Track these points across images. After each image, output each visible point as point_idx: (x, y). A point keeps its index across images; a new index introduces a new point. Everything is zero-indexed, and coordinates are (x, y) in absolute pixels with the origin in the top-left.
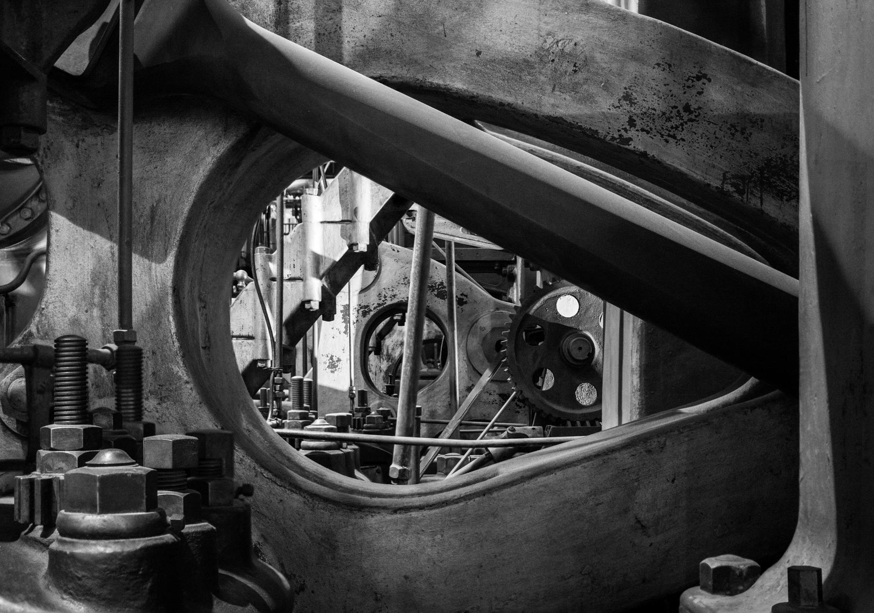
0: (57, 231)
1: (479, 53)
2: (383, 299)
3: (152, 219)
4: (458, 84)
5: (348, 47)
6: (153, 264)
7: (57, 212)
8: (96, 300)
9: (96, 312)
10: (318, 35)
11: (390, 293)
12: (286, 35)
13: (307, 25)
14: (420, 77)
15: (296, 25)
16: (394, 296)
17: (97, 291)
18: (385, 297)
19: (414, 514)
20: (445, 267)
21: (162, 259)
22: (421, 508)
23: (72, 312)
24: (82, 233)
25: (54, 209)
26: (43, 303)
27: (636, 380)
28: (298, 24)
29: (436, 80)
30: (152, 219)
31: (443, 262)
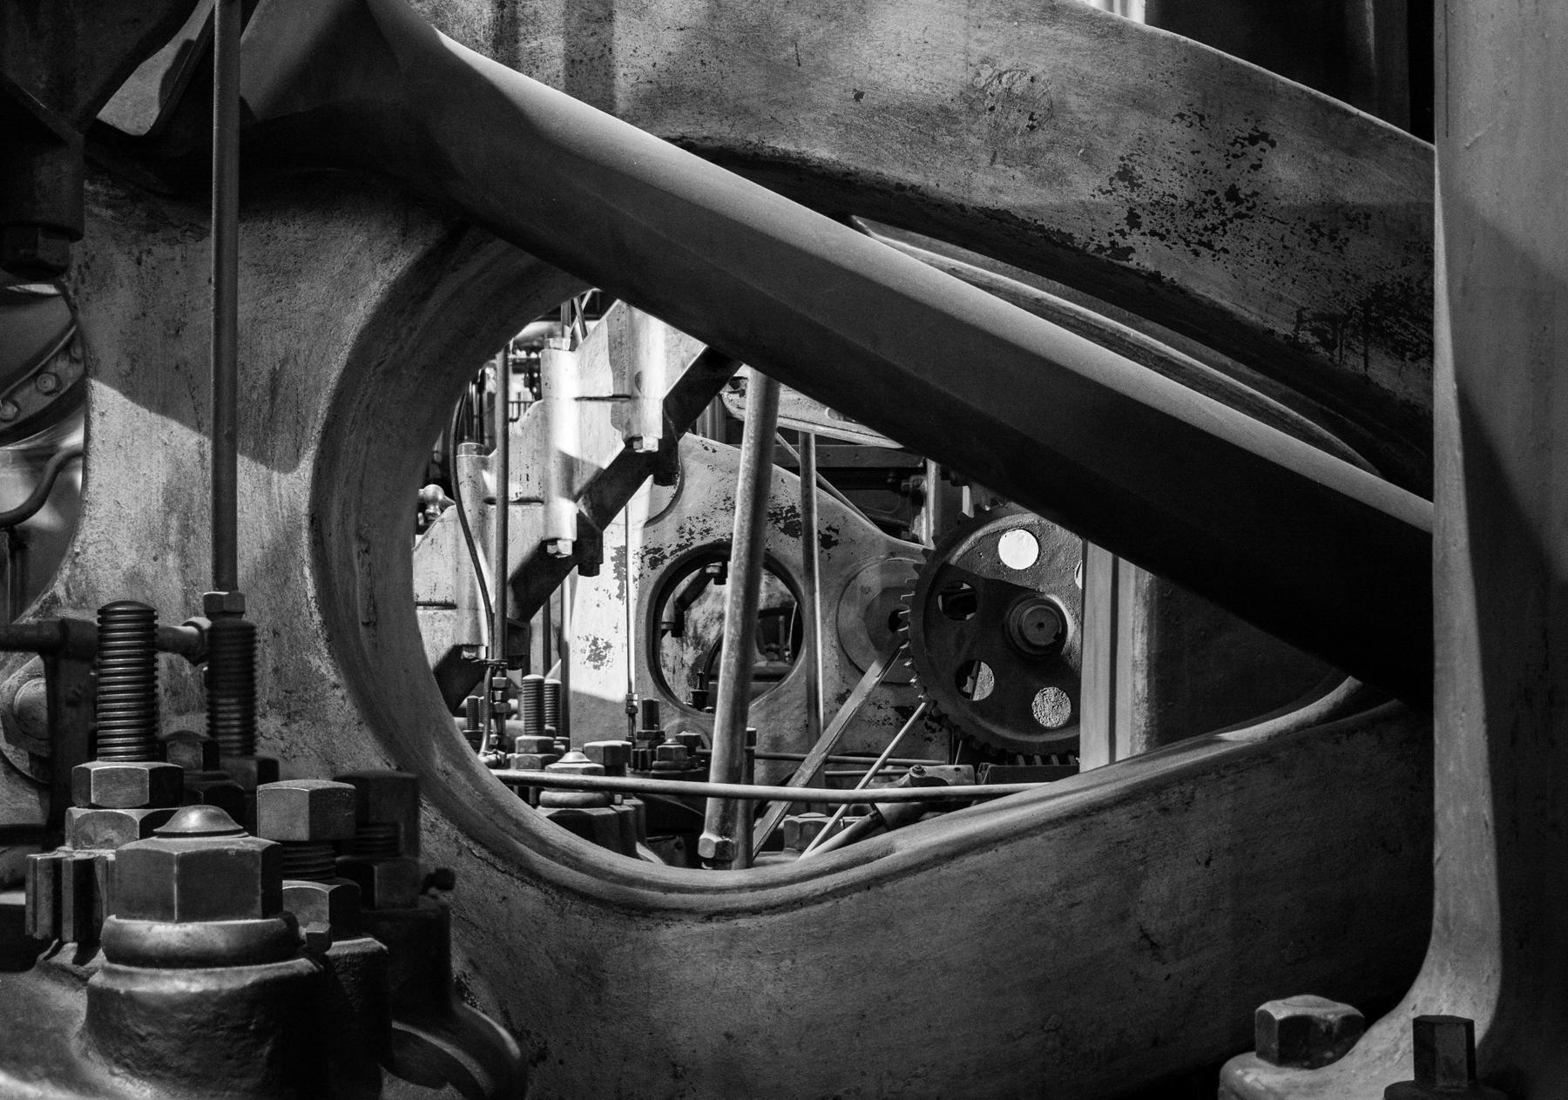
0: (103, 414)
1: (859, 96)
2: (688, 536)
3: (273, 392)
4: (822, 151)
5: (624, 85)
6: (275, 474)
7: (102, 380)
8: (172, 539)
9: (172, 560)
10: (571, 63)
11: (699, 526)
12: (513, 63)
13: (551, 44)
14: (753, 138)
15: (531, 44)
16: (708, 531)
17: (174, 523)
18: (691, 533)
19: (743, 922)
20: (798, 478)
21: (290, 465)
22: (755, 911)
23: (129, 559)
24: (146, 418)
25: (96, 375)
26: (78, 544)
27: (1141, 683)
28: (534, 44)
29: (783, 144)
30: (273, 392)
31: (795, 470)
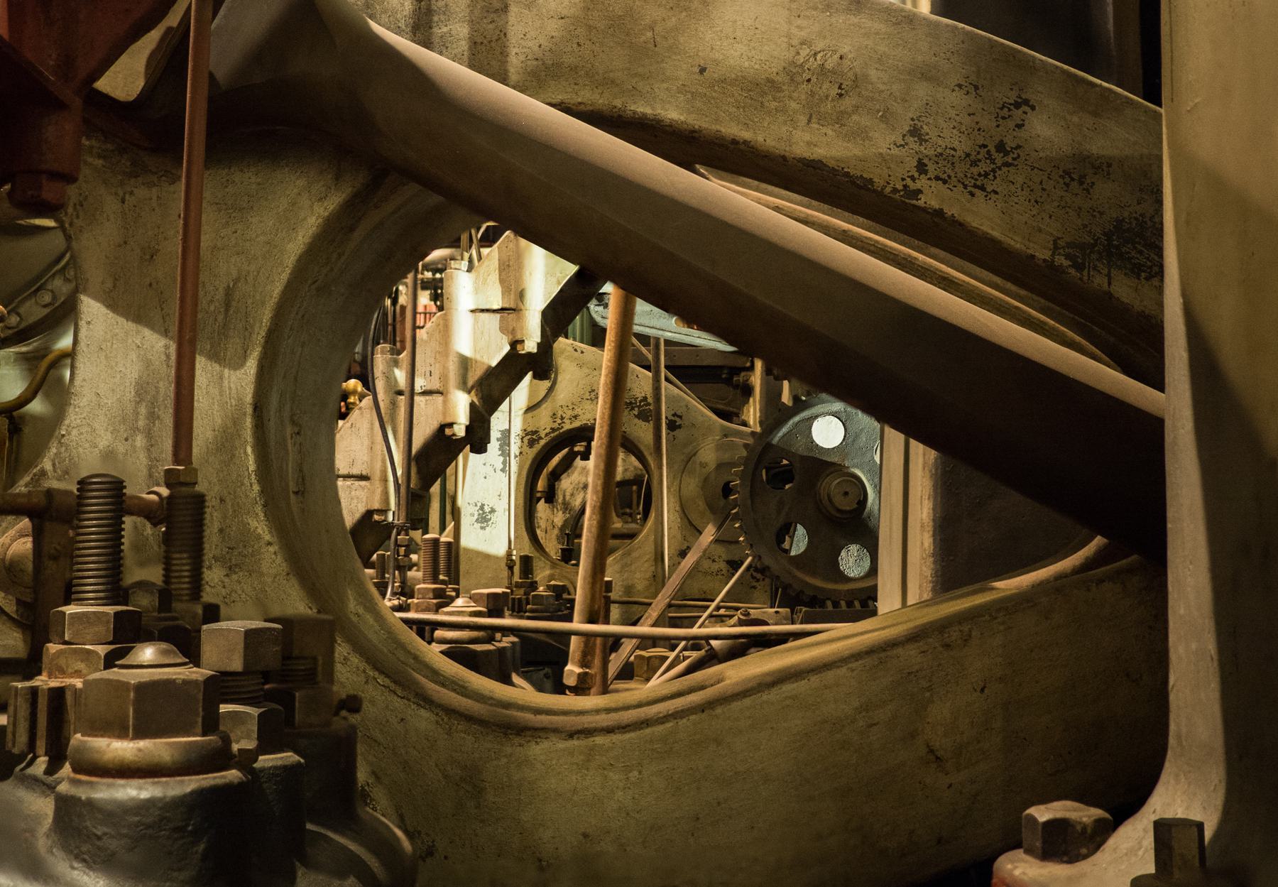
0: (89, 323)
1: (702, 70)
2: (559, 421)
3: (227, 306)
4: (673, 113)
5: (515, 62)
7: (89, 296)
8: (141, 423)
9: (140, 441)
10: (474, 44)
11: (569, 413)
12: (427, 44)
13: (458, 29)
14: (618, 103)
15: (438, 31)
18: (562, 418)
19: (599, 740)
21: (238, 364)
22: (609, 730)
24: (123, 325)
25: (85, 291)
26: (64, 427)
28: (445, 29)
29: (642, 108)
30: (227, 306)
31: (648, 368)
